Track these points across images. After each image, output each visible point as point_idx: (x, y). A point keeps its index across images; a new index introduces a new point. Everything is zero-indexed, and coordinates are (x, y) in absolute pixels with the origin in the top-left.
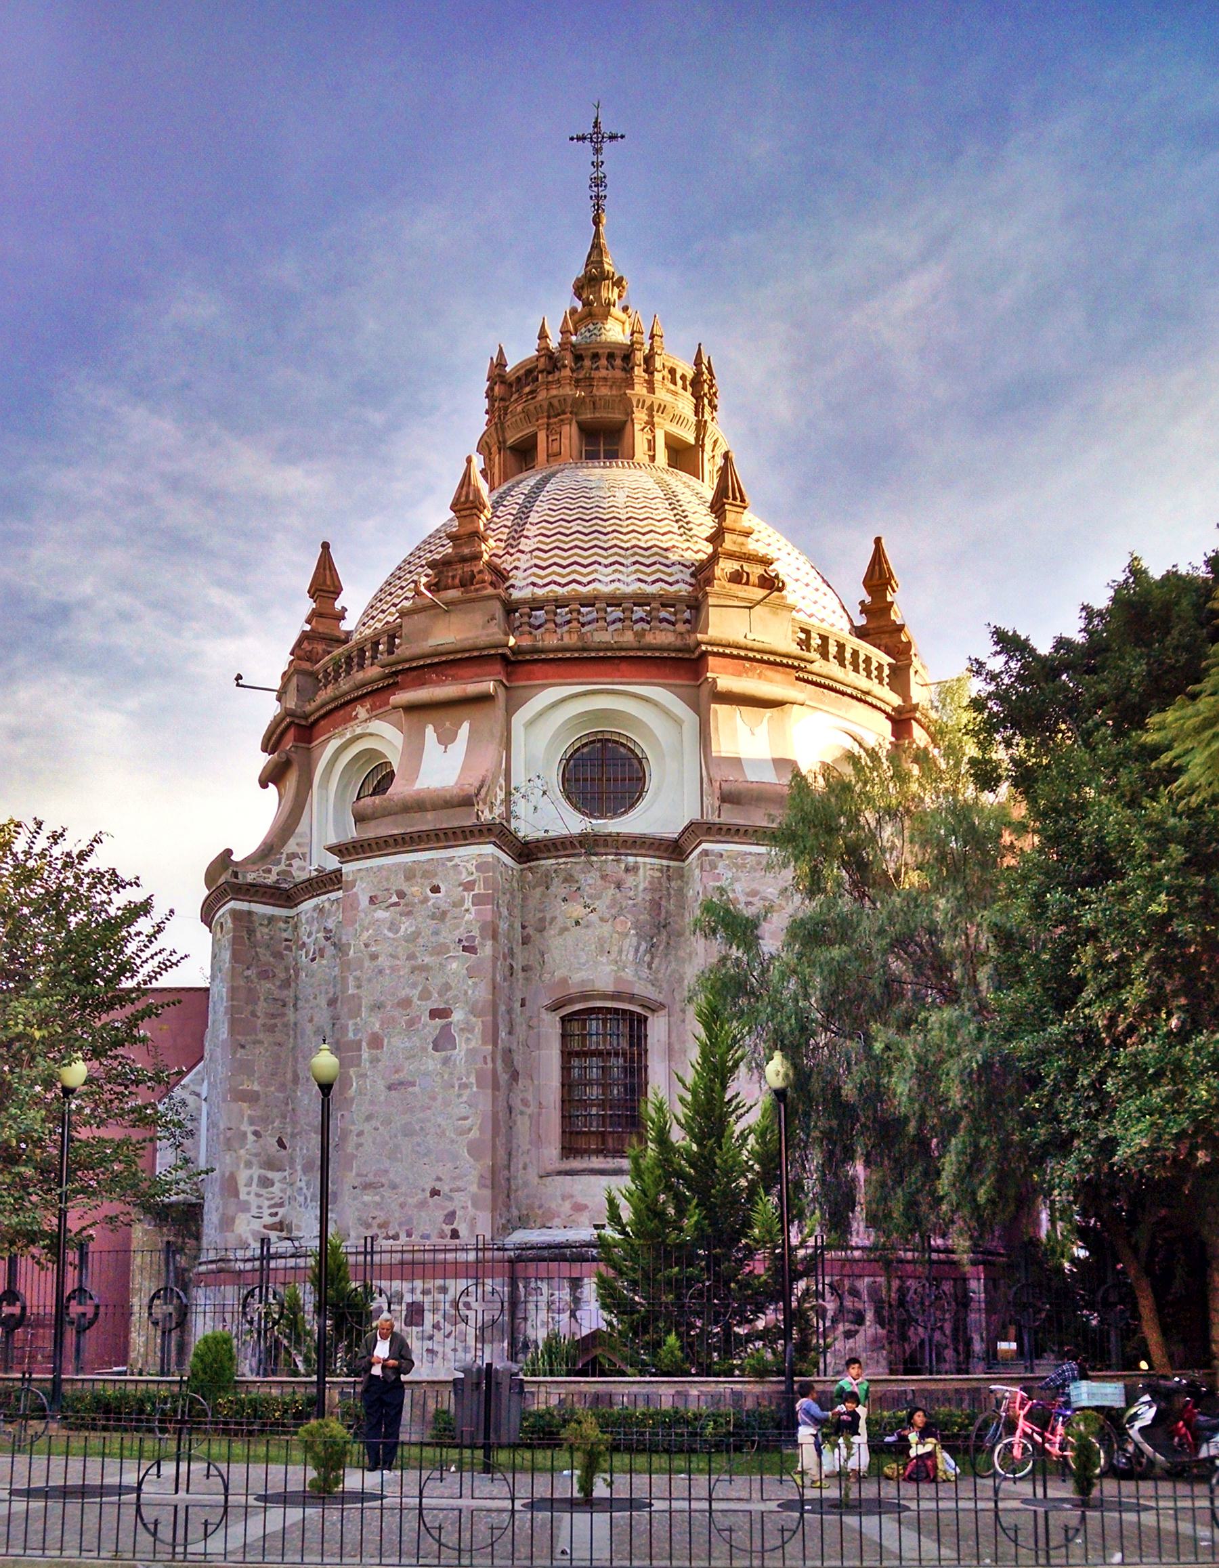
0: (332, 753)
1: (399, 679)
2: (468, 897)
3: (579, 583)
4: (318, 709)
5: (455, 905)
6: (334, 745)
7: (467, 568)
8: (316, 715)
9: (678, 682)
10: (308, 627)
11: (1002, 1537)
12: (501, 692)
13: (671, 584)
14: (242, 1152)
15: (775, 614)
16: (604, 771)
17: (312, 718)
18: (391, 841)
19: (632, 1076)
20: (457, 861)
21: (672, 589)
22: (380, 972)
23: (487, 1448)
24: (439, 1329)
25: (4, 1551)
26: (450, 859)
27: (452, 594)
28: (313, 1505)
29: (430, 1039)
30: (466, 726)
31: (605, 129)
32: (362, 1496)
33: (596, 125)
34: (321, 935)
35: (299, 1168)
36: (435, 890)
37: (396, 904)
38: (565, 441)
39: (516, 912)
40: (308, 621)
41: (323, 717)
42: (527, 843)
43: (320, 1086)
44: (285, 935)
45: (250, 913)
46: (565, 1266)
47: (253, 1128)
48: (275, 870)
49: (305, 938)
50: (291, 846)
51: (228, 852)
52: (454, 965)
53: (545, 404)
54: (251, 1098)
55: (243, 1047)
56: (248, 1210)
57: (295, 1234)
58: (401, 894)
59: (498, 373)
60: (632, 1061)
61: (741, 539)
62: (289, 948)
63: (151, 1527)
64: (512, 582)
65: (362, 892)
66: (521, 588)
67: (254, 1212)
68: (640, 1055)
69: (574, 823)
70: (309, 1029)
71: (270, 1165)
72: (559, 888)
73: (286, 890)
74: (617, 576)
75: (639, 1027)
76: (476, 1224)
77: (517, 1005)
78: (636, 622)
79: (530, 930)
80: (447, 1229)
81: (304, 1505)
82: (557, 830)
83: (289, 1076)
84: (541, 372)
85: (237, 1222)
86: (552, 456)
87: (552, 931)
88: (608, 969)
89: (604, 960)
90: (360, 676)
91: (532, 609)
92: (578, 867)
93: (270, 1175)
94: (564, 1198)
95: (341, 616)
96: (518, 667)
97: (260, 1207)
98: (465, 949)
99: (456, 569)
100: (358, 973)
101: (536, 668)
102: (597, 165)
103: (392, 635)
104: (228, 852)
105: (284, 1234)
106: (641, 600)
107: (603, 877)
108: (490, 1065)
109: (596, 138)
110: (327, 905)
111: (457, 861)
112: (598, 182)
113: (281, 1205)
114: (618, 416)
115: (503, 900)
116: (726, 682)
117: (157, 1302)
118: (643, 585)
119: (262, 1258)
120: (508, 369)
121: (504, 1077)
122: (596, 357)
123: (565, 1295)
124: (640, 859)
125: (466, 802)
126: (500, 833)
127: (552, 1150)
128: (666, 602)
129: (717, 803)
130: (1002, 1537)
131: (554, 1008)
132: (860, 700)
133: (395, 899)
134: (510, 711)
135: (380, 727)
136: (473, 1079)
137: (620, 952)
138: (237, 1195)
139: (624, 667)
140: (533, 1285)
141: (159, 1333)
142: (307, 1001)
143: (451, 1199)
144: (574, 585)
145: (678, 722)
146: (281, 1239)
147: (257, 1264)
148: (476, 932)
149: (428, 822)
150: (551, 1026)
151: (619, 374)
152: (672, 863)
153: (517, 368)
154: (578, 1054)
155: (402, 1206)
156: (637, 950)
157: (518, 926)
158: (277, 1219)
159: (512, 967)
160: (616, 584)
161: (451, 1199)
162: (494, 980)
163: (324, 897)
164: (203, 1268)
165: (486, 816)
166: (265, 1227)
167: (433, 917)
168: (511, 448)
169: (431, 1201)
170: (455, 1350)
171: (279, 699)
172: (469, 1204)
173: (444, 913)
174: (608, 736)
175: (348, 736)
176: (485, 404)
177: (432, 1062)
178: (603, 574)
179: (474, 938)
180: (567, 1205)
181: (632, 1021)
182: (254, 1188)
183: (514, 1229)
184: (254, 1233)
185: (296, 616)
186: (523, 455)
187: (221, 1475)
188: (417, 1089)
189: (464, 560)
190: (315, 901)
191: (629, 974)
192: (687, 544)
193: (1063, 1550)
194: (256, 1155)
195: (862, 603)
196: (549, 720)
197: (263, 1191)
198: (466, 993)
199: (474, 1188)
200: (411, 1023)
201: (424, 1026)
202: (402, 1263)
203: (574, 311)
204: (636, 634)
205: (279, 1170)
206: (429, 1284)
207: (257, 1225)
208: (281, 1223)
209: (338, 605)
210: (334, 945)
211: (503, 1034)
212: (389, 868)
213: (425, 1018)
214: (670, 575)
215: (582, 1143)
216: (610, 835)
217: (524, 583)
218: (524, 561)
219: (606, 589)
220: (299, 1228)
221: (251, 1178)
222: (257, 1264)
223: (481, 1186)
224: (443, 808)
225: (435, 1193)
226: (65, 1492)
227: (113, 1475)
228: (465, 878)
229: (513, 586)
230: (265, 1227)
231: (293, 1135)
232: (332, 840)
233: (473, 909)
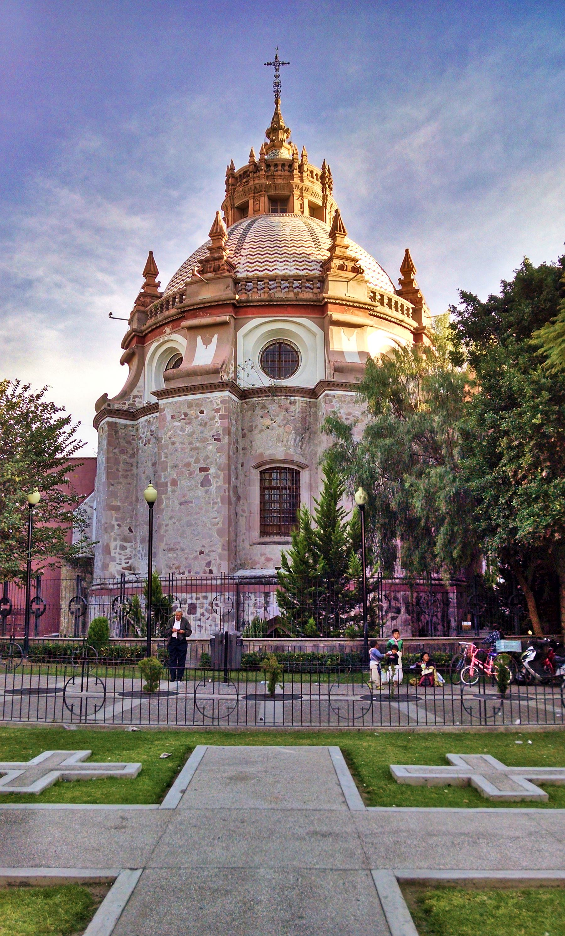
0: (154, 349)
1: (185, 314)
2: (217, 415)
3: (268, 270)
4: (147, 329)
5: (211, 419)
6: (155, 345)
7: (217, 263)
8: (147, 331)
9: (314, 316)
10: (143, 291)
11: (464, 712)
12: (232, 320)
13: (311, 271)
14: (112, 534)
15: (359, 284)
16: (280, 357)
17: (145, 333)
18: (181, 390)
19: (293, 499)
20: (212, 399)
21: (311, 273)
22: (176, 450)
23: (226, 671)
24: (204, 616)
25: (2, 719)
26: (209, 398)
27: (210, 275)
28: (145, 698)
29: (199, 482)
30: (216, 336)
31: (281, 60)
32: (168, 693)
33: (276, 58)
34: (149, 433)
35: (138, 541)
36: (202, 412)
37: (184, 419)
38: (262, 204)
39: (239, 422)
40: (143, 288)
41: (150, 332)
42: (244, 391)
43: (149, 503)
44: (132, 433)
45: (116, 423)
46: (262, 586)
47: (117, 523)
48: (128, 403)
49: (141, 435)
50: (135, 392)
51: (106, 395)
52: (211, 447)
53: (253, 187)
54: (116, 509)
55: (113, 485)
56: (115, 561)
57: (137, 572)
58: (186, 414)
59: (231, 173)
60: (293, 492)
61: (343, 250)
62: (134, 439)
63: (70, 707)
64: (237, 269)
65: (168, 413)
66: (241, 273)
67: (118, 561)
68: (296, 489)
69: (266, 381)
70: (143, 477)
71: (125, 540)
72: (259, 412)
73: (133, 413)
74: (286, 267)
75: (296, 476)
76: (221, 567)
77: (240, 466)
78: (295, 288)
79: (245, 431)
80: (207, 569)
81: (141, 697)
82: (258, 384)
83: (134, 498)
84: (251, 172)
85: (110, 566)
86: (256, 211)
87: (256, 431)
88: (282, 449)
89: (280, 445)
90: (167, 313)
91: (247, 282)
92: (268, 402)
93: (125, 544)
94: (261, 555)
95: (158, 286)
96: (240, 309)
97: (120, 559)
98: (215, 440)
99: (211, 264)
100: (166, 451)
101: (248, 310)
102: (277, 77)
103: (182, 294)
104: (106, 395)
105: (132, 572)
106: (297, 278)
107: (280, 407)
108: (227, 494)
109: (276, 64)
110: (151, 419)
111: (212, 399)
112: (277, 84)
113: (130, 558)
114: (286, 193)
115: (233, 417)
116: (337, 316)
117: (73, 603)
118: (298, 271)
119: (121, 583)
120: (235, 171)
121: (233, 499)
122: (276, 165)
123: (262, 600)
124: (296, 398)
125: (216, 371)
126: (232, 386)
127: (256, 533)
128: (309, 279)
129: (332, 372)
130: (464, 712)
131: (257, 467)
132: (398, 324)
133: (183, 416)
134: (236, 330)
135: (176, 337)
136: (219, 500)
137: (288, 441)
138: (110, 554)
139: (289, 309)
140: (247, 595)
141: (74, 618)
142: (142, 464)
143: (209, 555)
144: (266, 271)
145: (314, 335)
146: (130, 574)
147: (119, 585)
148: (220, 432)
149: (198, 381)
150: (255, 475)
151: (287, 173)
152: (311, 400)
153: (240, 171)
154: (268, 488)
155: (186, 559)
156: (295, 440)
157: (240, 429)
158: (128, 565)
159: (237, 448)
160: (286, 271)
161: (209, 555)
162: (229, 454)
163: (150, 416)
164: (94, 588)
165: (225, 378)
166: (123, 568)
167: (201, 425)
168: (237, 208)
169: (200, 556)
170: (211, 625)
171: (129, 324)
172: (218, 558)
173: (206, 423)
174: (282, 341)
175: (161, 341)
176: (225, 187)
177: (200, 492)
178: (280, 266)
179: (220, 434)
180: (263, 558)
181: (293, 473)
182: (118, 550)
183: (238, 569)
184: (118, 571)
185: (137, 285)
186: (242, 211)
187: (102, 684)
188: (193, 505)
189: (215, 259)
190: (146, 418)
191: (291, 451)
192: (318, 252)
193: (493, 718)
194: (119, 535)
195: (400, 279)
196: (254, 334)
197: (122, 552)
198: (216, 460)
199: (220, 551)
200: (190, 474)
201: (197, 475)
202: (186, 585)
203: (266, 144)
204: (295, 294)
205: (129, 542)
206: (199, 595)
207: (119, 568)
208: (130, 567)
209: (157, 280)
210: (155, 438)
211: (233, 479)
212: (180, 402)
213: (197, 472)
214: (311, 266)
215: (270, 530)
216: (282, 387)
217: (243, 270)
218: (243, 260)
219: (281, 273)
220: (139, 569)
221: (116, 546)
222: (119, 585)
223: (223, 549)
224: (213, 373)
225: (202, 553)
226: (30, 691)
227: (52, 683)
228: (215, 407)
229: (238, 271)
230: (123, 568)
231: (136, 526)
232: (154, 389)
233: (219, 421)
